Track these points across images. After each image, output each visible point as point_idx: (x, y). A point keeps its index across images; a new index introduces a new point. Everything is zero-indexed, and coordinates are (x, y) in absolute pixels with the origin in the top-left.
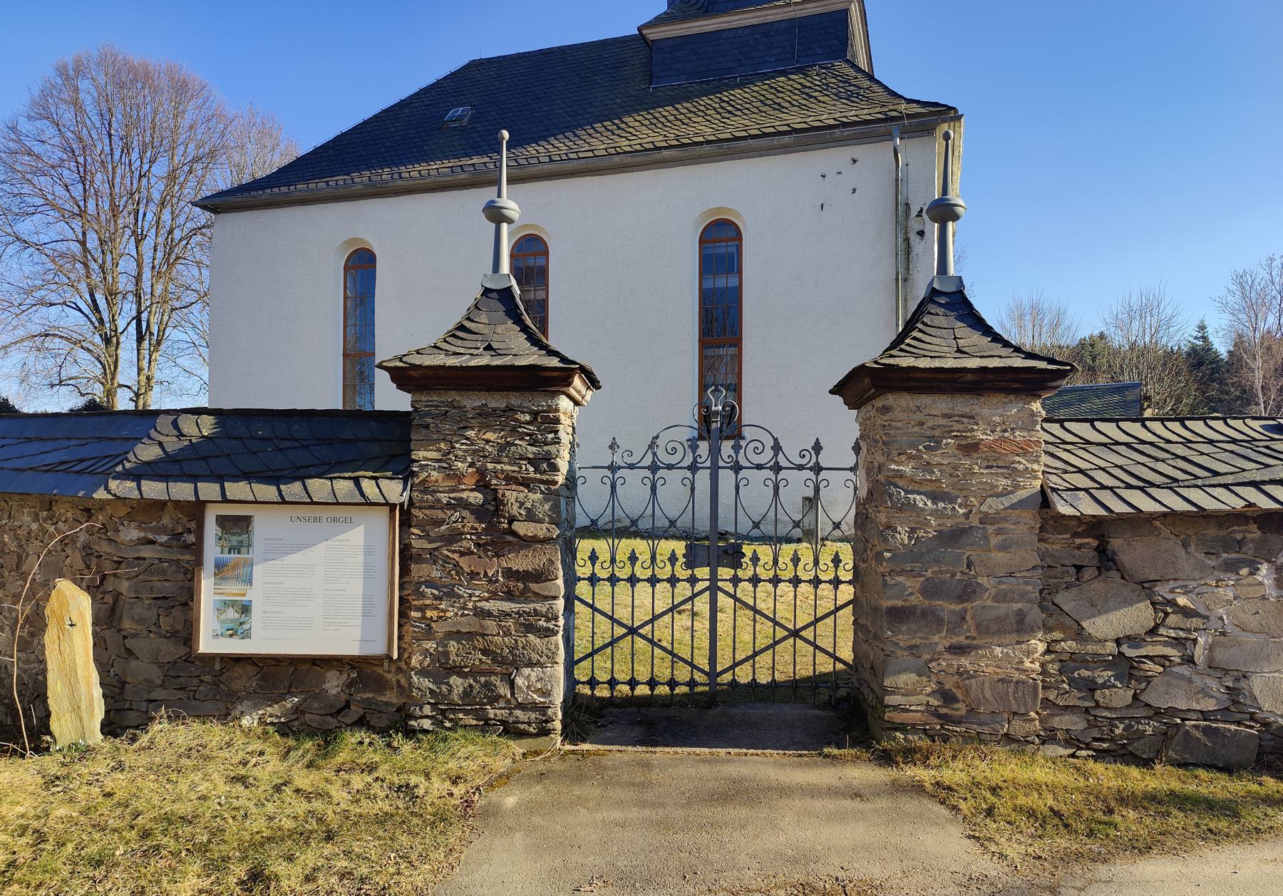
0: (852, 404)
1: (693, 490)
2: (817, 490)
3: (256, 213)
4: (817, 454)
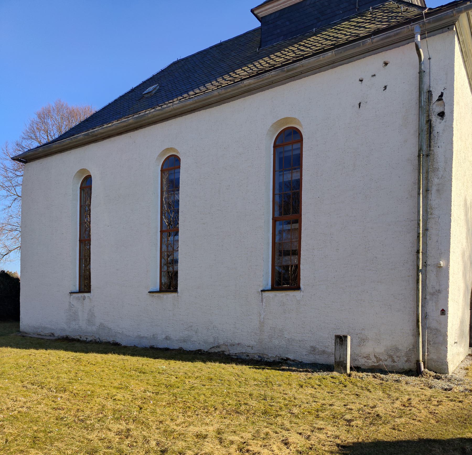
3: (113, 139)
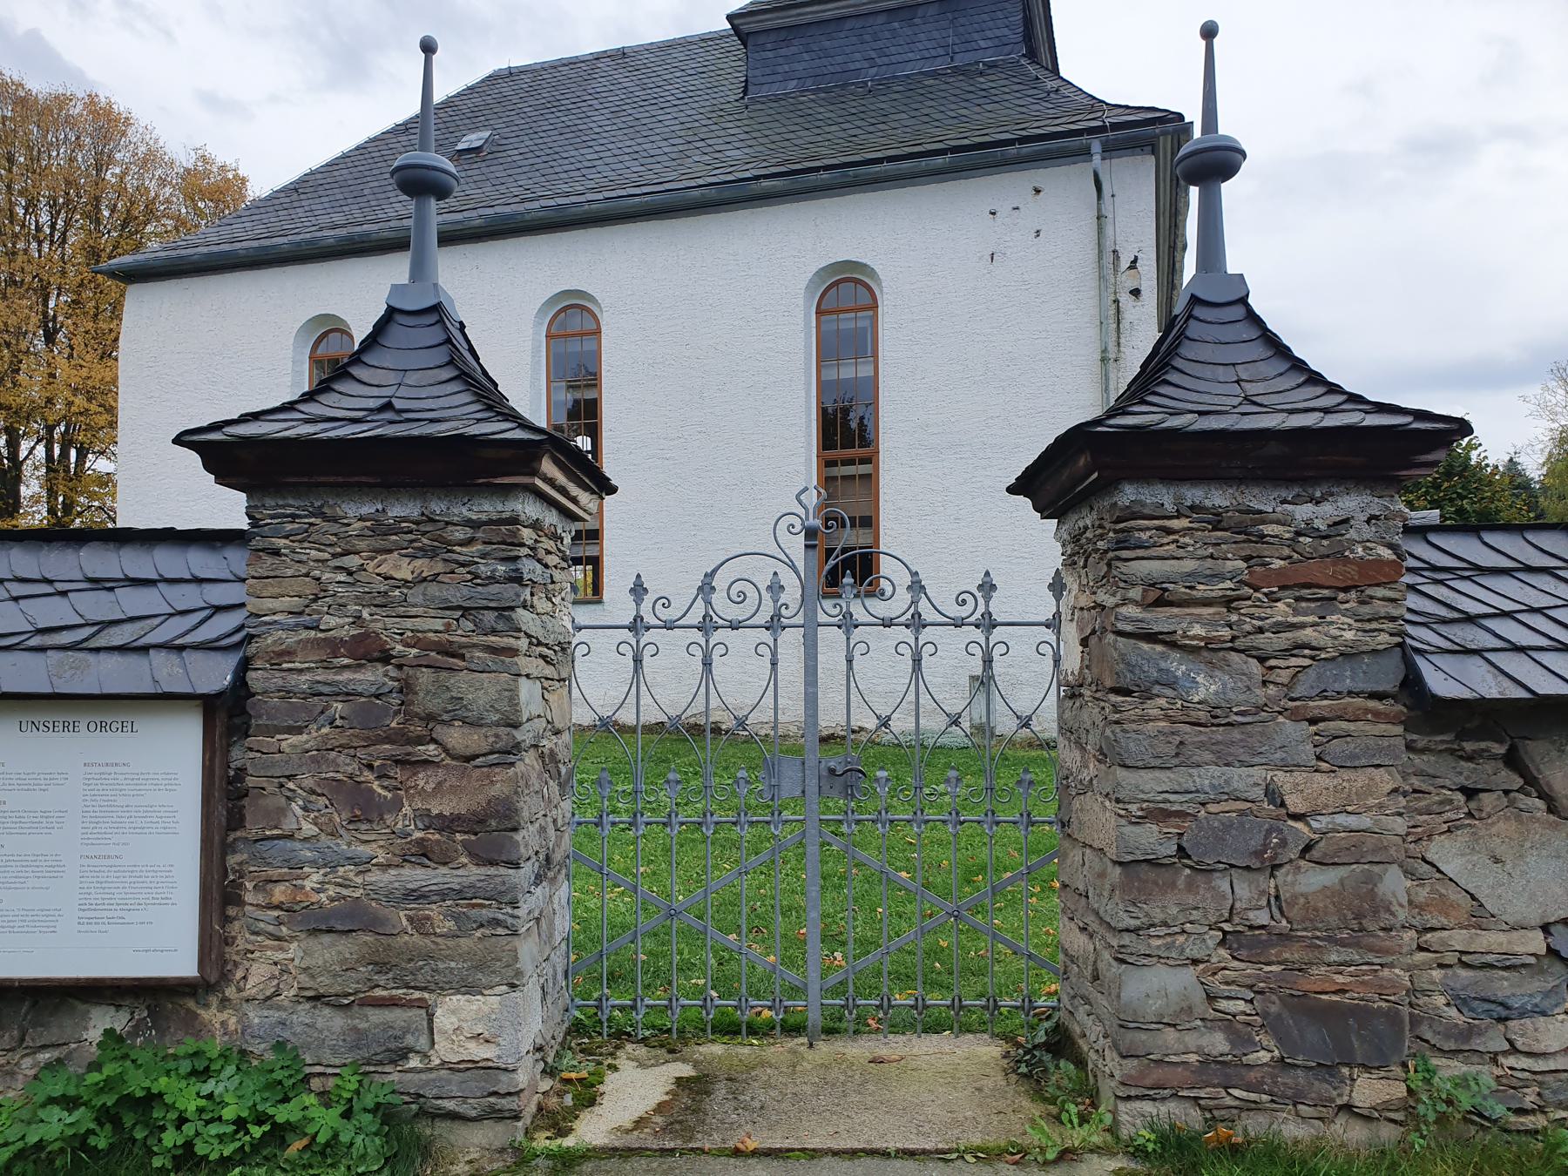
0: (1046, 509)
1: (774, 664)
2: (988, 662)
4: (987, 599)
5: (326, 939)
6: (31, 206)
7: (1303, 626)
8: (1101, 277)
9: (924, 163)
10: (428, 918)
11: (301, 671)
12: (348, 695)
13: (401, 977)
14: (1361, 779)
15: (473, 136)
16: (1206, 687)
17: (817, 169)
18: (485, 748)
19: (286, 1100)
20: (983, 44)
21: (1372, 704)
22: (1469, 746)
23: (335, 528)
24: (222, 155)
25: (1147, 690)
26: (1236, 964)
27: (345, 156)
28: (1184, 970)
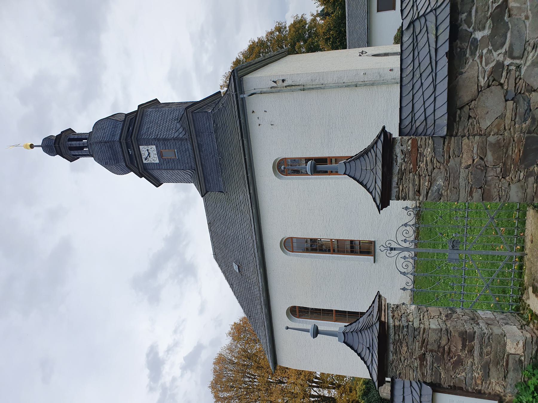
5: (490, 373)
6: (245, 383)
7: (426, 160)
8: (279, 92)
9: (246, 147)
10: (487, 352)
11: (427, 372)
12: (433, 363)
13: (501, 360)
14: (465, 147)
15: (235, 267)
16: (440, 182)
17: (248, 177)
18: (446, 337)
19: (529, 387)
20: (208, 124)
21: (446, 144)
22: (457, 119)
23: (395, 361)
24: (228, 329)
25: (440, 195)
26: (510, 175)
27: (240, 302)
28: (511, 188)
